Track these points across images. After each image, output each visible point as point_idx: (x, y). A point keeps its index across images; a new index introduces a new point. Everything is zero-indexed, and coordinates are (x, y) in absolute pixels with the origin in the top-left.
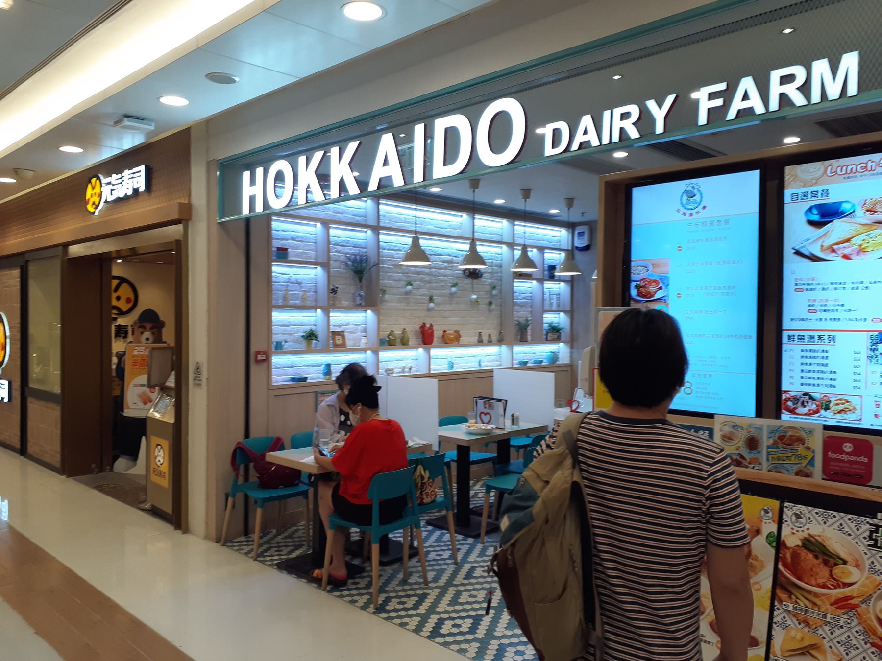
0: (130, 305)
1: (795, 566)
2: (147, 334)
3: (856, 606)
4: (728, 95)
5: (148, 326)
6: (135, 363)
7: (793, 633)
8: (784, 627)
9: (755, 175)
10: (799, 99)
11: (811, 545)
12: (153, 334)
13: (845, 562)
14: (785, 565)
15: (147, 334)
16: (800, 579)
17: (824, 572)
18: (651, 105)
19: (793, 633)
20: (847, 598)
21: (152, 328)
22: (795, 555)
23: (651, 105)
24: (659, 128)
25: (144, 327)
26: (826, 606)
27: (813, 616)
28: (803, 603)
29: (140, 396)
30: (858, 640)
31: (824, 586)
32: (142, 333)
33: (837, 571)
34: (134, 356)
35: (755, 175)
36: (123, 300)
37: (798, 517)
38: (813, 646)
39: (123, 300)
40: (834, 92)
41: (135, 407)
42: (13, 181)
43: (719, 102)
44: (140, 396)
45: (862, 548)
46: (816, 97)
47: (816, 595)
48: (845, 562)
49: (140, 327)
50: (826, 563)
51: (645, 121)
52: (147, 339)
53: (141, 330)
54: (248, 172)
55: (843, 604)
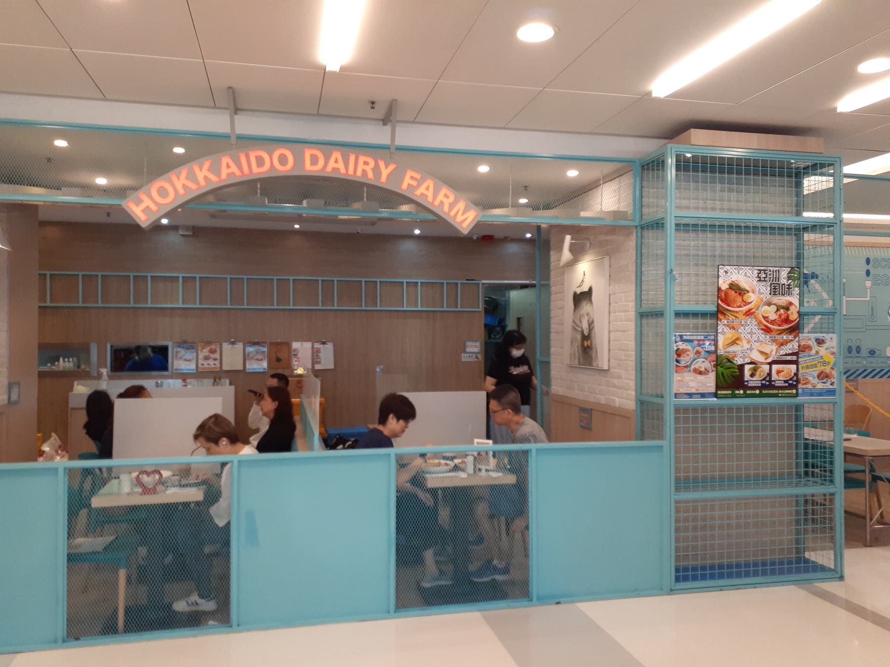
1: (726, 300)
3: (753, 313)
4: (420, 183)
7: (727, 335)
8: (723, 333)
10: (446, 208)
11: (734, 287)
13: (748, 292)
14: (722, 301)
16: (729, 306)
17: (739, 299)
18: (382, 165)
19: (727, 335)
20: (750, 310)
22: (726, 293)
23: (382, 165)
24: (384, 178)
26: (741, 316)
27: (736, 323)
28: (731, 318)
30: (755, 329)
31: (740, 307)
33: (745, 297)
37: (726, 272)
38: (738, 339)
40: (459, 218)
43: (414, 183)
45: (755, 283)
46: (452, 214)
47: (737, 312)
48: (748, 292)
50: (740, 294)
51: (377, 170)
55: (749, 313)
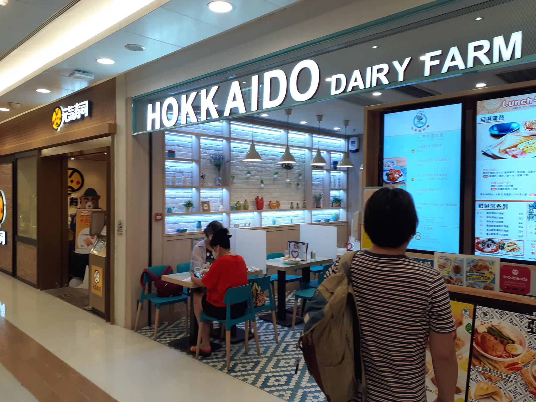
0: (79, 185)
1: (483, 344)
2: (89, 203)
3: (520, 369)
4: (442, 58)
5: (90, 198)
6: (82, 221)
7: (482, 385)
8: (477, 381)
9: (459, 107)
10: (485, 60)
11: (493, 331)
12: (93, 203)
13: (513, 342)
14: (477, 344)
15: (89, 203)
16: (486, 352)
17: (501, 348)
18: (396, 64)
19: (482, 385)
20: (515, 364)
21: (92, 200)
22: (483, 337)
23: (396, 64)
24: (401, 78)
25: (88, 199)
26: (502, 369)
27: (494, 375)
28: (488, 367)
29: (85, 241)
30: (521, 389)
31: (501, 357)
32: (86, 203)
33: (508, 347)
34: (82, 216)
35: (459, 107)
36: (75, 182)
37: (485, 314)
38: (494, 393)
39: (75, 182)
40: (507, 56)
41: (82, 247)
42: (8, 110)
43: (437, 62)
44: (85, 241)
45: (524, 333)
46: (496, 59)
47: (496, 362)
48: (513, 342)
49: (85, 199)
50: (502, 342)
51: (392, 73)
52: (90, 206)
53: (86, 200)
54: (151, 105)
55: (512, 367)
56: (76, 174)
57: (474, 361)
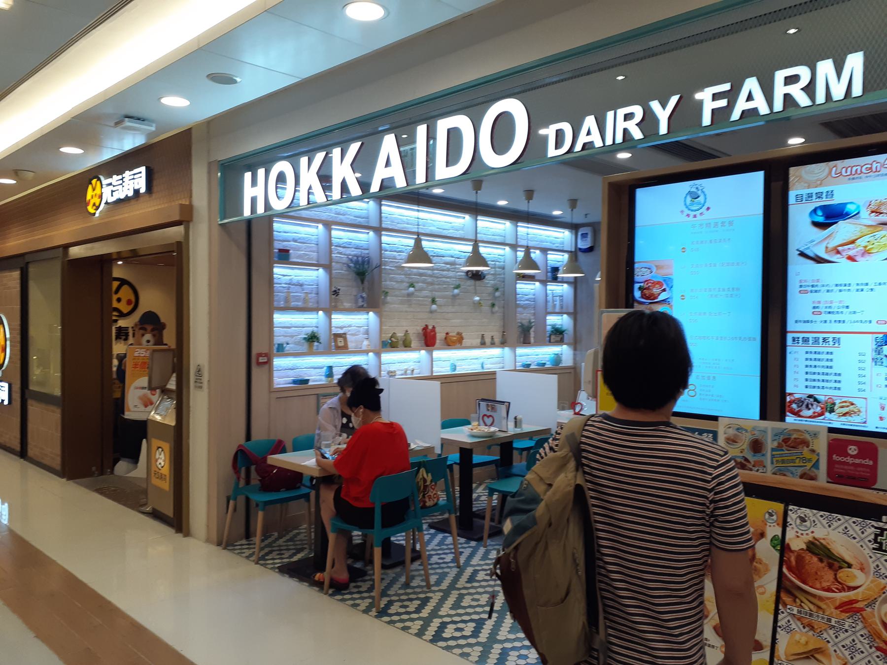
0: (131, 307)
1: (799, 570)
2: (148, 336)
3: (861, 610)
4: (732, 96)
5: (149, 328)
6: (135, 366)
7: (797, 637)
8: (789, 630)
9: (759, 177)
10: (803, 100)
11: (816, 548)
12: (154, 336)
13: (850, 566)
14: (790, 569)
15: (148, 336)
16: (804, 582)
17: (828, 576)
18: (655, 105)
19: (797, 637)
20: (852, 602)
21: (152, 330)
22: (800, 558)
23: (655, 105)
24: (663, 129)
25: (145, 329)
26: (831, 610)
27: (818, 620)
28: (807, 606)
29: (141, 398)
30: (863, 644)
31: (829, 590)
32: (143, 335)
33: (841, 575)
34: (135, 358)
35: (759, 177)
36: (124, 302)
37: (803, 520)
38: (818, 650)
39: (124, 302)
40: (838, 93)
41: (136, 409)
42: (13, 182)
43: (723, 103)
44: (141, 398)
45: (867, 552)
46: (820, 98)
47: (821, 599)
48: (850, 566)
49: (141, 329)
50: (830, 566)
51: (648, 122)
52: (148, 341)
53: (142, 332)
54: (250, 173)
55: (848, 607)
56: (125, 288)
57: (785, 597)
